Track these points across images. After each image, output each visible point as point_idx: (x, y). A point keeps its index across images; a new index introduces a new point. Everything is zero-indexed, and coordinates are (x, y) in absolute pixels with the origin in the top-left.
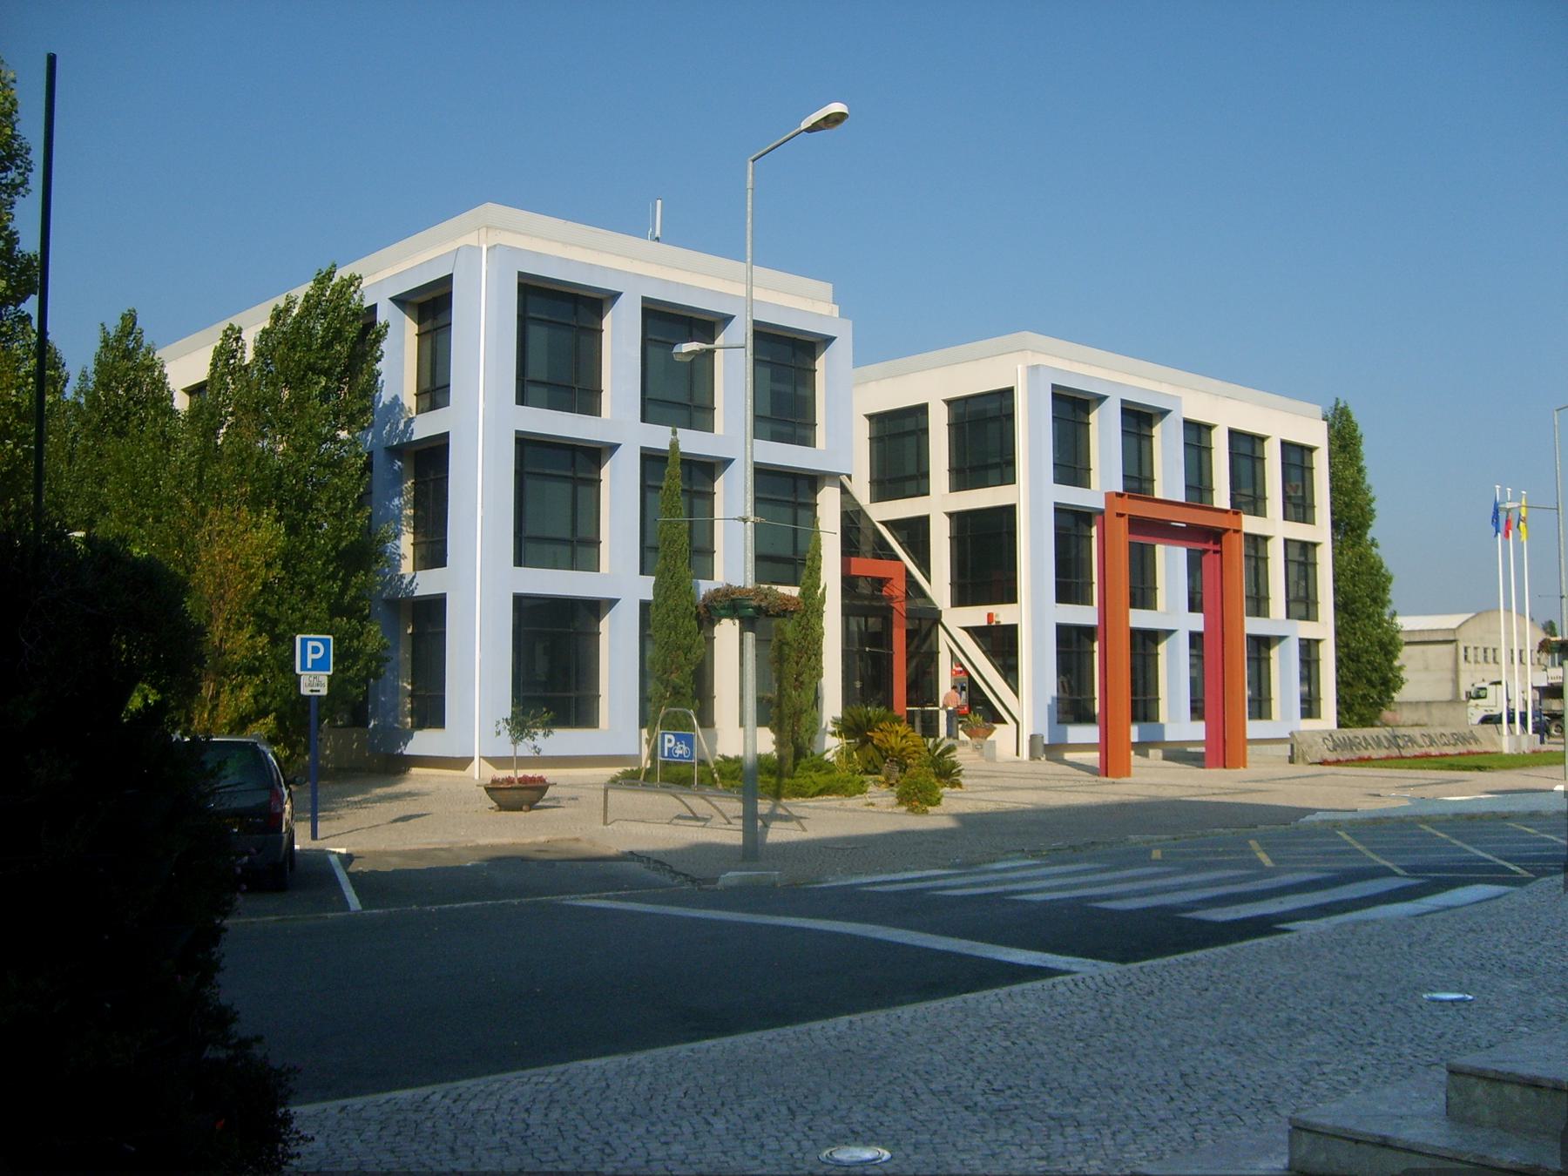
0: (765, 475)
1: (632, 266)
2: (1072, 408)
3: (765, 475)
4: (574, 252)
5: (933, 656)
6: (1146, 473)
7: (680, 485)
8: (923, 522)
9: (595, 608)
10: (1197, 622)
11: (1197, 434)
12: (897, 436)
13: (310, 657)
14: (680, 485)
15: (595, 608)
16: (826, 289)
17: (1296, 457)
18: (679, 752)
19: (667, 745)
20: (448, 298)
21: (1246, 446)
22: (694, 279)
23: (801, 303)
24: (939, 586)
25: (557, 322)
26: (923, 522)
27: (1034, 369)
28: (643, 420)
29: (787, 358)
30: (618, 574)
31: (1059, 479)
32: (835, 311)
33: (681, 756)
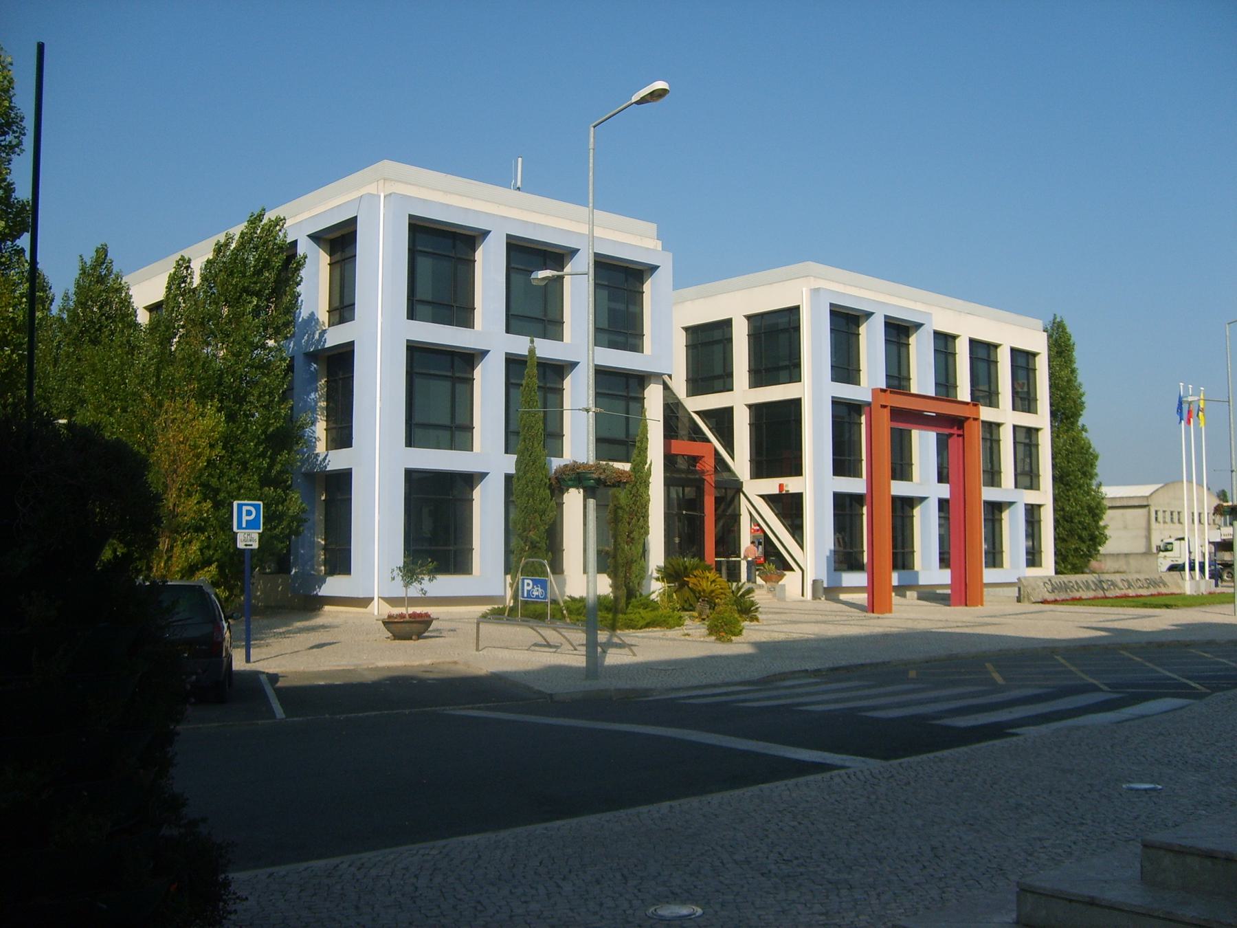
0: (603, 375)
1: (499, 210)
2: (845, 322)
3: (603, 375)
4: (453, 199)
5: (736, 518)
7: (536, 383)
9: (469, 480)
10: (944, 491)
11: (944, 342)
12: (707, 344)
13: (245, 518)
14: (536, 383)
15: (469, 480)
16: (652, 228)
17: (1023, 360)
19: (526, 588)
21: (983, 352)
22: (547, 220)
23: (632, 239)
24: (741, 462)
25: (440, 254)
27: (815, 292)
29: (621, 282)
30: (488, 453)
33: (537, 597)
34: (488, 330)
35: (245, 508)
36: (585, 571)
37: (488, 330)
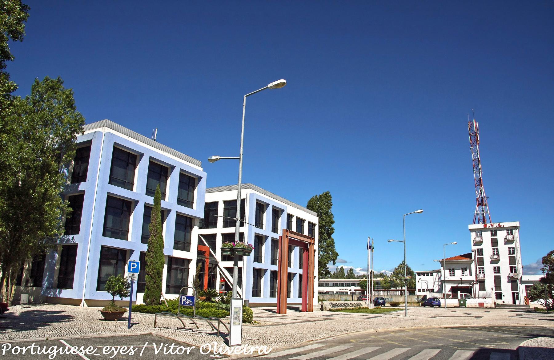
0: (179, 216)
1: (149, 149)
2: (261, 207)
3: (179, 216)
4: (132, 141)
5: (215, 277)
6: (190, 199)
7: (154, 216)
8: (214, 236)
9: (189, 261)
10: (145, 248)
11: (290, 217)
12: (211, 208)
13: (132, 268)
14: (154, 216)
15: (189, 261)
16: (199, 163)
17: (311, 226)
18: (188, 303)
19: (183, 300)
20: (90, 147)
21: (300, 222)
22: (166, 155)
23: (194, 168)
24: (218, 256)
25: (124, 161)
26: (214, 236)
27: (252, 195)
28: (110, 183)
29: (188, 182)
30: (133, 241)
31: (112, 181)
32: (201, 169)
33: (189, 304)
34: (138, 190)
35: (132, 263)
36: (489, 312)
37: (138, 190)
